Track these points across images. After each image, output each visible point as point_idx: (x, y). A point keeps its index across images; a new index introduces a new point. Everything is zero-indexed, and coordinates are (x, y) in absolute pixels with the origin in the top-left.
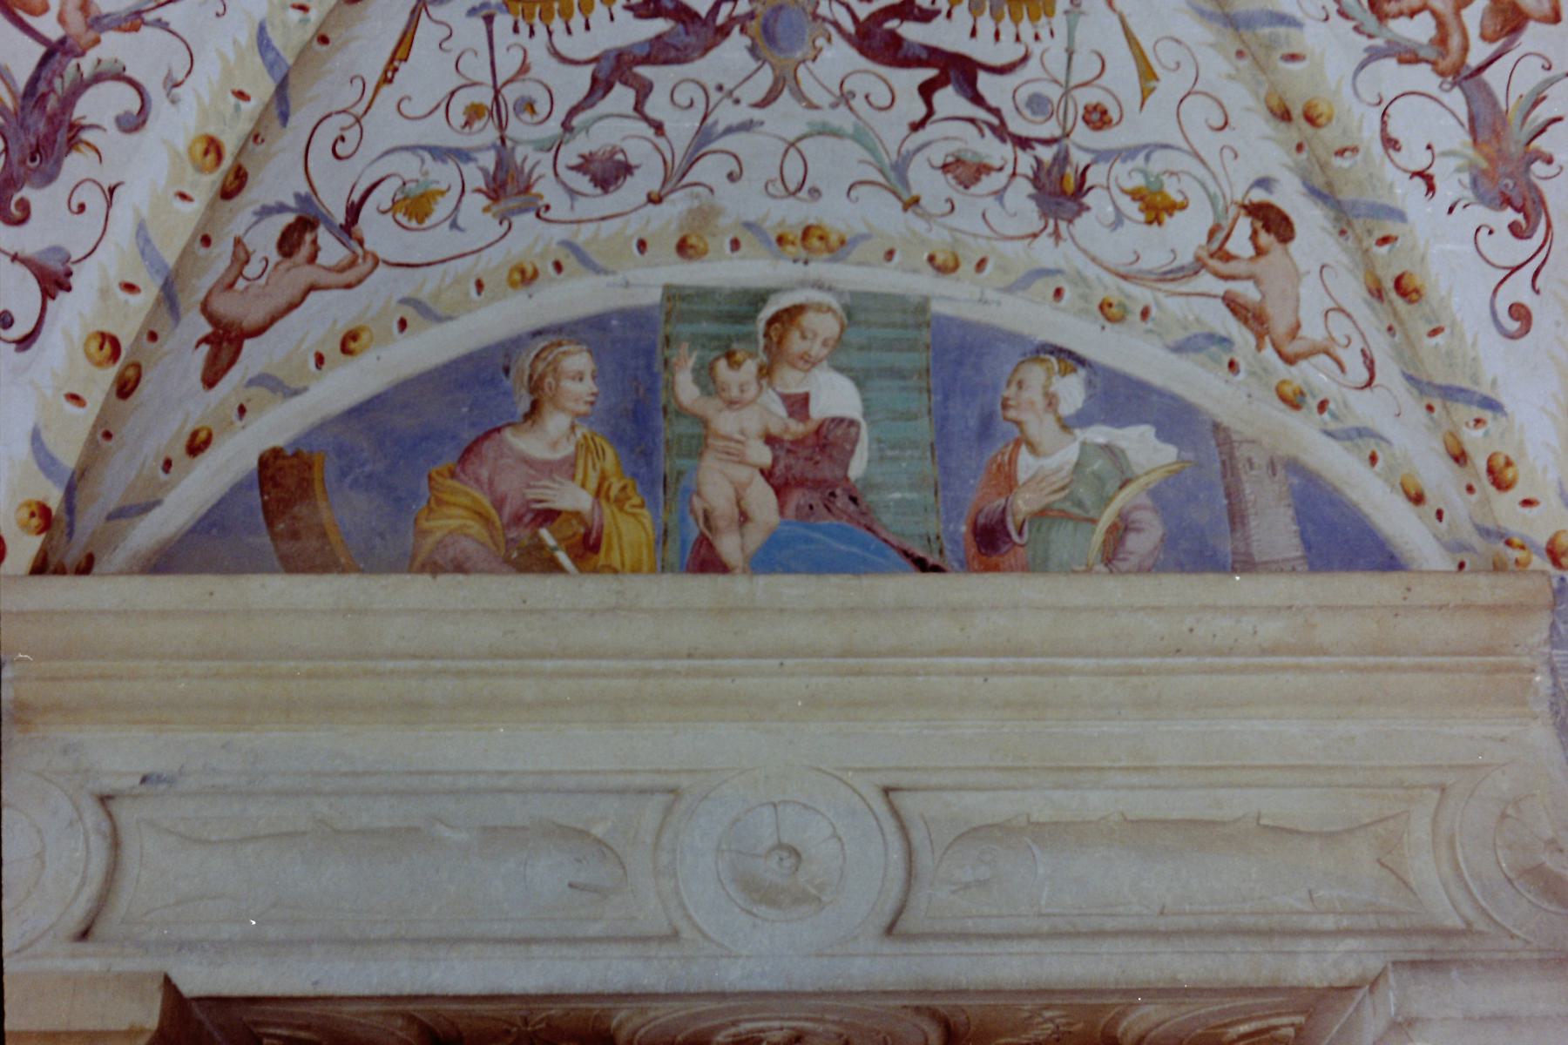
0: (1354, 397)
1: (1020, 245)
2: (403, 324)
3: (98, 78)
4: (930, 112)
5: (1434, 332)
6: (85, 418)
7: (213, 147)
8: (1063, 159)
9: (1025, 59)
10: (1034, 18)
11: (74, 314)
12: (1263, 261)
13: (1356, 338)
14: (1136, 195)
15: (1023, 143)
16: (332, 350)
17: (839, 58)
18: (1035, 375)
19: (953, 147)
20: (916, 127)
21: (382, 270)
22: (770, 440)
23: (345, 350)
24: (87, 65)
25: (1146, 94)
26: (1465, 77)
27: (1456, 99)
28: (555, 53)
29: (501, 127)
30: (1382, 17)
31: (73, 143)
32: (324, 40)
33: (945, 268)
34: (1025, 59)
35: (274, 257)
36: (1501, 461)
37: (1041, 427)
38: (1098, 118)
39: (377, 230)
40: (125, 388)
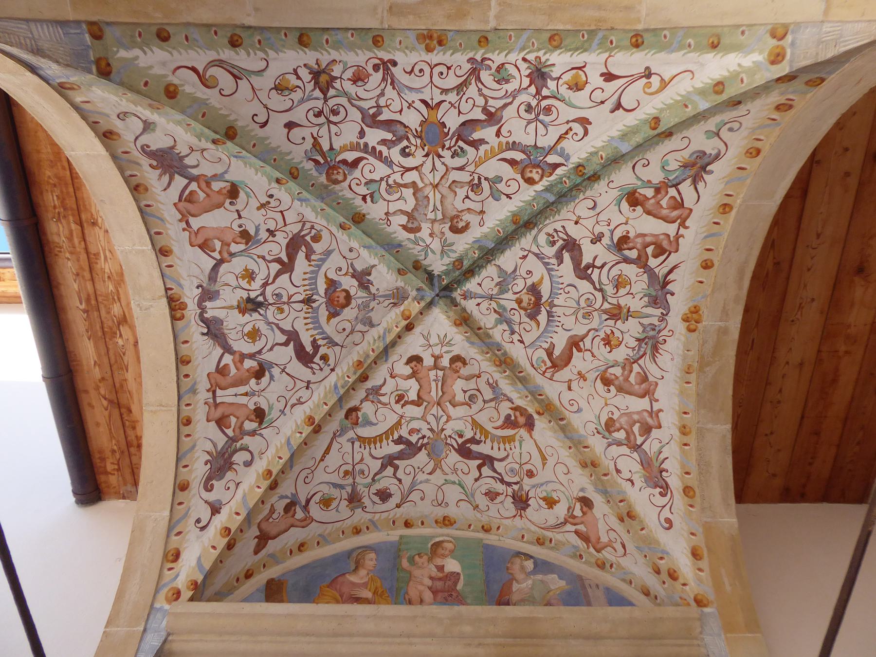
0: (621, 560)
1: (509, 521)
2: (318, 543)
3: (241, 449)
4: (481, 474)
5: (642, 529)
6: (215, 553)
7: (270, 472)
8: (521, 488)
9: (508, 456)
10: (509, 443)
11: (220, 521)
12: (585, 517)
13: (618, 537)
14: (544, 499)
15: (509, 484)
16: (295, 550)
17: (454, 458)
18: (517, 561)
19: (488, 486)
20: (476, 480)
21: (314, 523)
22: (431, 578)
23: (300, 550)
24: (238, 445)
25: (544, 464)
26: (637, 448)
27: (635, 455)
28: (371, 455)
29: (354, 479)
30: (610, 432)
31: (230, 468)
32: (306, 444)
33: (486, 530)
34: (508, 456)
35: (282, 513)
36: (672, 571)
37: (520, 576)
38: (530, 474)
39: (315, 511)
40: (230, 546)
